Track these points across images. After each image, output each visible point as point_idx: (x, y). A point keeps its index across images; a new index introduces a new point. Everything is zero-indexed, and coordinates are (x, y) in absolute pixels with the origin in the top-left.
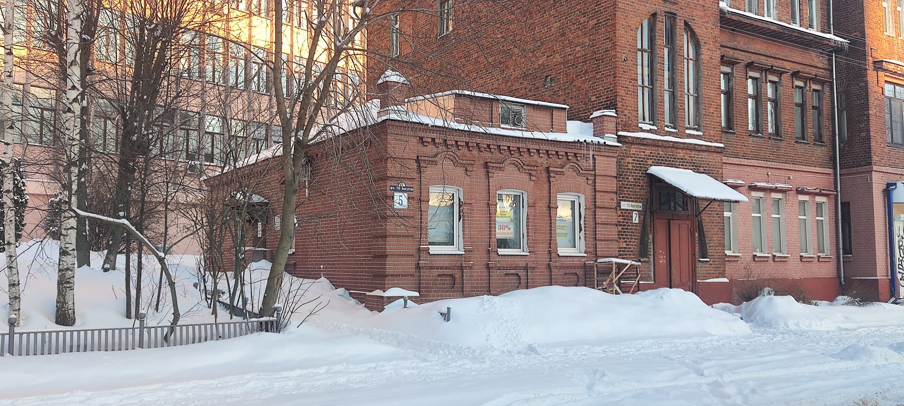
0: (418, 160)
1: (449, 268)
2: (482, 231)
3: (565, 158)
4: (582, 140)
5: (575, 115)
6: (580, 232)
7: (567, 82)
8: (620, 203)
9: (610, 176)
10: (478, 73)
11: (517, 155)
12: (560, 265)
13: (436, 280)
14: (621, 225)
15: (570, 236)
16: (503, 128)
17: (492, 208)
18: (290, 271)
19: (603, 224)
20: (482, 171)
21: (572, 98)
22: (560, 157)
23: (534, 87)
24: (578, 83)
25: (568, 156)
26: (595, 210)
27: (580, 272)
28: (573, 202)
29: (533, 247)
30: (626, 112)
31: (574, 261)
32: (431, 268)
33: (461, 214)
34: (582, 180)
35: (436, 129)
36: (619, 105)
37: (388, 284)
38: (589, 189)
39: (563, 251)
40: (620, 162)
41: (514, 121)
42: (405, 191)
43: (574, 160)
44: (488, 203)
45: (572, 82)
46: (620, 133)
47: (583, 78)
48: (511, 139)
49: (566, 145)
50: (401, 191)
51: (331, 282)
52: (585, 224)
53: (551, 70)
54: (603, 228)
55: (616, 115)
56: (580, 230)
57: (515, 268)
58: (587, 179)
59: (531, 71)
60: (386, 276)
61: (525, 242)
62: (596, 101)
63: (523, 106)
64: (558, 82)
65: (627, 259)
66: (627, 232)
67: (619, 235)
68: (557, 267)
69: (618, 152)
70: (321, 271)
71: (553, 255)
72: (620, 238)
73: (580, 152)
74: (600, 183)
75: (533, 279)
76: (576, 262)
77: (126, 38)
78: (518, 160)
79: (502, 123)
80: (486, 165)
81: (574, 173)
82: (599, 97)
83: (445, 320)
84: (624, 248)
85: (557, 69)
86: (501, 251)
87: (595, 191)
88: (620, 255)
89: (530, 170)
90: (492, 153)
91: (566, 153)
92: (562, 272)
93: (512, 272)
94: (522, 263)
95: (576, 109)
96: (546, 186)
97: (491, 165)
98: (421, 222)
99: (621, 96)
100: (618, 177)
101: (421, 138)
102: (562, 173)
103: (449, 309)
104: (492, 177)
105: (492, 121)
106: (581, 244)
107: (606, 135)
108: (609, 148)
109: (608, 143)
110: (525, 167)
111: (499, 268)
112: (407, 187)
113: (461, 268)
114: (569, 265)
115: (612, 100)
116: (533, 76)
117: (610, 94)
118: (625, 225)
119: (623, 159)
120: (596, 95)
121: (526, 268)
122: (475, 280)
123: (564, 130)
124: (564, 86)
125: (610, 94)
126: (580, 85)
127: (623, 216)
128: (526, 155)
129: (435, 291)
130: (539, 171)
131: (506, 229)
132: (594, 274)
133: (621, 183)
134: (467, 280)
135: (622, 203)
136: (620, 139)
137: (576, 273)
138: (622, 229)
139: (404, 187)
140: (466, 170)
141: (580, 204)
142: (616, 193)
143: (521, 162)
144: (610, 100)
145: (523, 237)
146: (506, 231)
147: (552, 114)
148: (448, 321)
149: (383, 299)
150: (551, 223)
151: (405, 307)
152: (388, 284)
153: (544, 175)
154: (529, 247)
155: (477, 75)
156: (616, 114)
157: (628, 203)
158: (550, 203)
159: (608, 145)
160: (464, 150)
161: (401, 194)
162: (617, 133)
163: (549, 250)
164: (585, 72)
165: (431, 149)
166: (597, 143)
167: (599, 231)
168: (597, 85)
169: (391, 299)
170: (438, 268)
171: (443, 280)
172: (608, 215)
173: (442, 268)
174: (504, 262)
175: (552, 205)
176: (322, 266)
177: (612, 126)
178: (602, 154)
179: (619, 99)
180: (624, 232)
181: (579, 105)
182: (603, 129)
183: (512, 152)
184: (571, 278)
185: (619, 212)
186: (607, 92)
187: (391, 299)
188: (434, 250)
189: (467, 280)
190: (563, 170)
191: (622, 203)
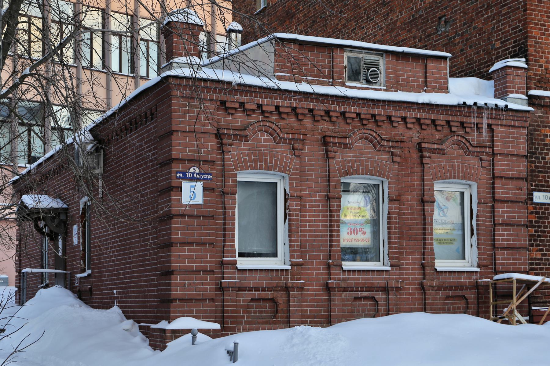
0: (218, 136)
1: (269, 289)
2: (318, 236)
3: (446, 130)
4: (470, 102)
5: (475, 71)
6: (471, 237)
7: (465, 24)
8: (532, 194)
9: (518, 155)
10: (357, 21)
11: (372, 126)
12: (438, 284)
13: (248, 306)
14: (534, 227)
15: (458, 244)
16: (350, 87)
17: (334, 203)
18: (87, 299)
19: (507, 225)
20: (319, 150)
21: (471, 47)
22: (439, 128)
23: (425, 34)
24: (478, 25)
25: (450, 127)
26: (493, 205)
27: (471, 295)
28: (462, 194)
29: (397, 258)
30: (542, 61)
31: (460, 278)
32: (240, 289)
33: (287, 211)
34: (472, 161)
35: (249, 89)
36: (531, 51)
37: (175, 312)
38: (483, 174)
39: (441, 265)
40: (532, 134)
41: (367, 77)
42: (198, 180)
43: (461, 132)
44: (327, 195)
45: (472, 22)
46: (533, 92)
47: (486, 16)
48: (361, 102)
49: (447, 111)
50: (191, 179)
51: (124, 312)
52: (478, 225)
53: (445, 8)
54: (505, 230)
55: (526, 66)
56: (472, 234)
57: (370, 289)
58: (481, 160)
59: (421, 12)
60: (171, 301)
61: (386, 251)
62: (501, 47)
63: (381, 55)
64: (453, 25)
65: (537, 274)
66: (544, 236)
67: (530, 240)
68: (433, 287)
69: (528, 119)
70: (114, 298)
71: (428, 270)
72: (532, 245)
73: (468, 120)
74: (502, 165)
75: (396, 305)
76: (463, 280)
77: (236, 61)
78: (372, 133)
79: (350, 79)
80: (324, 141)
81: (461, 151)
82: (504, 41)
83: (231, 360)
84: (539, 259)
85: (453, 6)
86: (348, 265)
87: (494, 177)
88: (532, 269)
89: (392, 147)
90: (334, 123)
91: (448, 122)
92: (441, 294)
93: (365, 294)
94: (379, 282)
95: (476, 62)
96: (418, 169)
97: (331, 140)
98: (225, 224)
99: (535, 37)
100: (530, 155)
101: (223, 103)
102: (441, 152)
103: (236, 345)
104: (333, 158)
105: (333, 76)
106: (472, 253)
107: (511, 95)
108: (514, 114)
109: (511, 106)
110: (384, 143)
111: (345, 290)
112: (203, 174)
113: (287, 289)
114: (452, 285)
115: (522, 44)
116: (423, 19)
117: (518, 36)
118: (539, 227)
119: (537, 131)
120: (501, 39)
121: (386, 289)
122: (308, 306)
123: (444, 89)
124: (461, 30)
125: (518, 36)
126: (481, 26)
127: (537, 213)
128: (386, 126)
129: (247, 323)
130: (407, 149)
131: (359, 233)
132: (489, 298)
133: (533, 165)
134: (295, 306)
135: (536, 194)
136: (532, 100)
137: (464, 296)
138: (535, 231)
139: (197, 174)
140: (293, 148)
141: (471, 196)
142: (527, 180)
143: (377, 136)
144: (518, 45)
145: (384, 245)
146: (360, 236)
147: (426, 66)
148: (234, 362)
149: (165, 333)
150: (425, 224)
151: (193, 344)
152: (175, 312)
153: (415, 155)
154: (391, 258)
155: (356, 25)
156: (527, 64)
157: (545, 194)
158: (424, 196)
159: (512, 110)
160: (291, 120)
161: (193, 183)
162: (527, 92)
163: (423, 264)
164: (487, 6)
165: (239, 119)
166: (494, 107)
167: (500, 235)
168: (502, 25)
169: (177, 333)
170: (250, 289)
171: (260, 307)
172: (513, 212)
173: (257, 289)
174: (352, 281)
175: (426, 198)
176: (115, 291)
177: (520, 81)
178: (504, 123)
179: (530, 42)
180: (539, 236)
181: (479, 56)
182: (506, 87)
183: (365, 122)
184: (456, 303)
185: (531, 208)
186: (515, 33)
187: (177, 333)
188: (243, 263)
189: (295, 306)
190: (444, 146)
191: (536, 194)
